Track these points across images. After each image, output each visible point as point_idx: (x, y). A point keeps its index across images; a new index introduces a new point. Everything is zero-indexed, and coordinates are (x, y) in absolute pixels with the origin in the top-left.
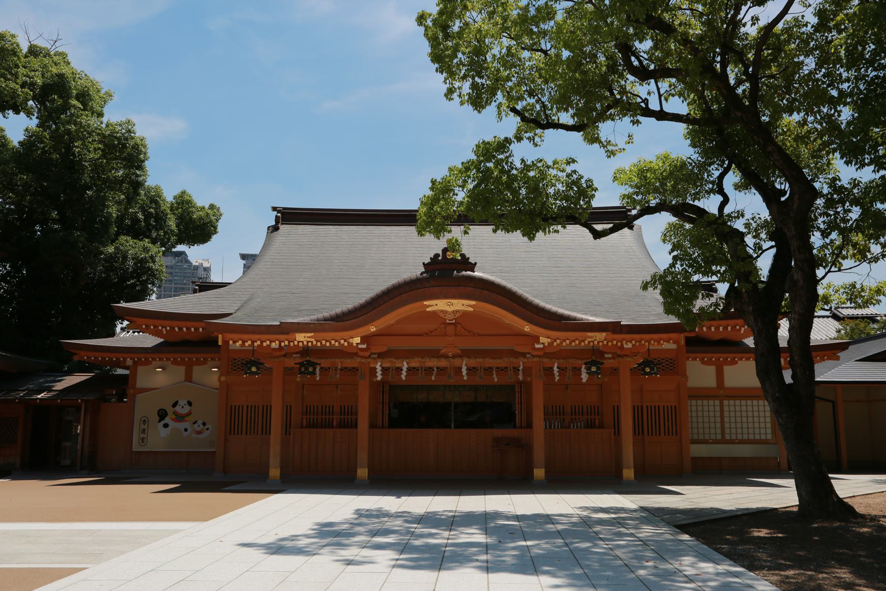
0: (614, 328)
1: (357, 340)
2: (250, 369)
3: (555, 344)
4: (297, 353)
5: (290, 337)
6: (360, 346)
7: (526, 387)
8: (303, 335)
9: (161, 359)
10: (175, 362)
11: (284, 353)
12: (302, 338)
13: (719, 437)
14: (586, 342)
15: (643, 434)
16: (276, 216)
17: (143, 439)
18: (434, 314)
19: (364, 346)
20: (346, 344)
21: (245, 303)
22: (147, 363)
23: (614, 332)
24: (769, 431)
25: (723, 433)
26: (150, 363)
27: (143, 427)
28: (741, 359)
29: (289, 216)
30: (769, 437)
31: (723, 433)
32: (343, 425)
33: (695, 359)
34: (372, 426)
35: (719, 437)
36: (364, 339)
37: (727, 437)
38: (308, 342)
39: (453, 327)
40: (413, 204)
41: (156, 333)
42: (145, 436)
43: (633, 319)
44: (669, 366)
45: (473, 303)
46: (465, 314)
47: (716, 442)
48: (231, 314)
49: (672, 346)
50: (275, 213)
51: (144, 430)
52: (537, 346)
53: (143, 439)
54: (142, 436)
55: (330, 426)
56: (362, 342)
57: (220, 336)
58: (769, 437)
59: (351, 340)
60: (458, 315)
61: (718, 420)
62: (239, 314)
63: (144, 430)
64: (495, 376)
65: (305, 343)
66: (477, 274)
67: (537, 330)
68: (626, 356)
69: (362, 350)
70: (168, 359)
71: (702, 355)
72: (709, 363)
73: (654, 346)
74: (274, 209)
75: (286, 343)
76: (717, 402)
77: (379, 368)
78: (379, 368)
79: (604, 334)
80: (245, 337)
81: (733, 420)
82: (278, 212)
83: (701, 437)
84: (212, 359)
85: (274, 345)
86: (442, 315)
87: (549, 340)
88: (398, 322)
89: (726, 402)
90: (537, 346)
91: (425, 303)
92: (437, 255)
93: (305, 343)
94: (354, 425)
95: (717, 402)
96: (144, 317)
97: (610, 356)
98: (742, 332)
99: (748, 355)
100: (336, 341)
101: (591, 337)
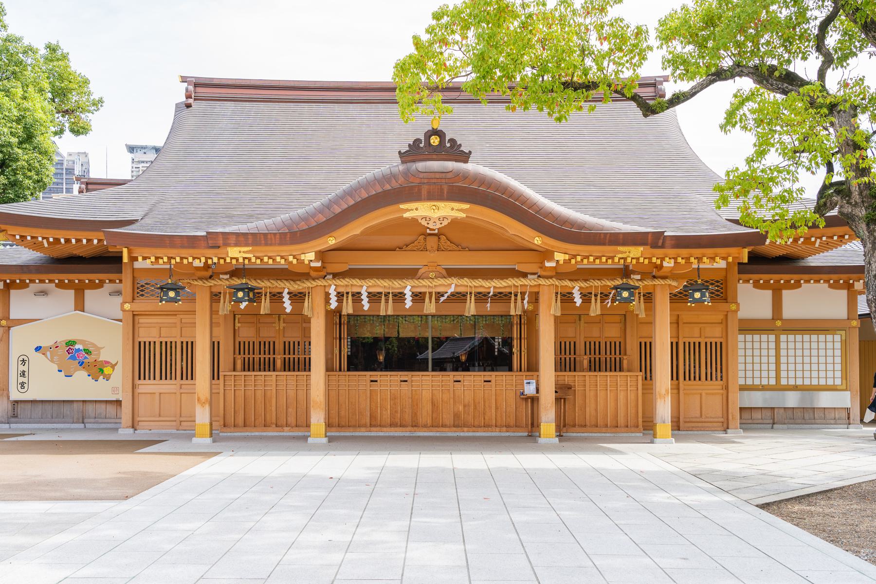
0: (655, 240)
1: (311, 256)
2: (166, 294)
3: (573, 261)
4: (226, 273)
5: (220, 252)
6: (312, 264)
7: (530, 319)
8: (237, 249)
9: (42, 281)
10: (61, 285)
11: (209, 273)
12: (236, 253)
13: (773, 382)
14: (616, 260)
15: (677, 379)
16: (187, 90)
17: (22, 384)
18: (414, 221)
19: (319, 264)
20: (295, 261)
21: (154, 205)
22: (23, 285)
23: (654, 246)
24: (838, 374)
25: (778, 377)
26: (27, 286)
27: (21, 368)
28: (808, 281)
29: (203, 91)
30: (838, 382)
31: (778, 377)
32: (288, 366)
33: (748, 281)
34: (329, 368)
35: (773, 382)
36: (321, 255)
37: (784, 382)
38: (244, 258)
39: (436, 238)
40: (385, 75)
41: (35, 245)
42: (25, 380)
43: (678, 228)
44: (720, 290)
45: (466, 206)
46: (455, 222)
47: (763, 388)
48: (137, 220)
49: (721, 264)
50: (186, 84)
51: (24, 372)
52: (548, 264)
53: (22, 384)
54: (21, 380)
55: (270, 366)
56: (317, 259)
57: (125, 251)
58: (838, 382)
59: (303, 257)
60: (445, 223)
61: (783, 360)
62: (147, 220)
63: (24, 372)
64: (489, 305)
65: (241, 260)
66: (470, 167)
67: (551, 243)
68: (664, 278)
69: (316, 269)
70: (51, 281)
71: (756, 277)
72: (765, 286)
73: (706, 264)
74: (184, 79)
75: (215, 260)
76: (772, 338)
77: (332, 291)
78: (332, 291)
79: (641, 249)
80: (159, 252)
81: (764, 360)
82: (189, 83)
83: (757, 382)
84: (111, 281)
85: (197, 263)
86: (424, 223)
87: (567, 257)
88: (362, 233)
89: (783, 338)
90: (548, 264)
91: (402, 206)
92: (417, 141)
93: (241, 260)
94: (306, 365)
95: (772, 338)
96: (603, 244)
97: (638, 277)
98: (817, 245)
99: (816, 276)
100: (270, 258)
101: (622, 252)
